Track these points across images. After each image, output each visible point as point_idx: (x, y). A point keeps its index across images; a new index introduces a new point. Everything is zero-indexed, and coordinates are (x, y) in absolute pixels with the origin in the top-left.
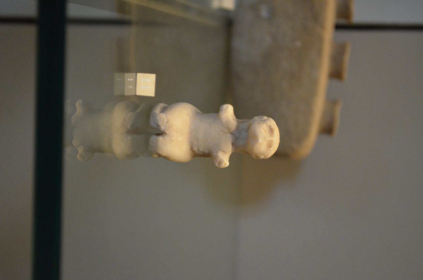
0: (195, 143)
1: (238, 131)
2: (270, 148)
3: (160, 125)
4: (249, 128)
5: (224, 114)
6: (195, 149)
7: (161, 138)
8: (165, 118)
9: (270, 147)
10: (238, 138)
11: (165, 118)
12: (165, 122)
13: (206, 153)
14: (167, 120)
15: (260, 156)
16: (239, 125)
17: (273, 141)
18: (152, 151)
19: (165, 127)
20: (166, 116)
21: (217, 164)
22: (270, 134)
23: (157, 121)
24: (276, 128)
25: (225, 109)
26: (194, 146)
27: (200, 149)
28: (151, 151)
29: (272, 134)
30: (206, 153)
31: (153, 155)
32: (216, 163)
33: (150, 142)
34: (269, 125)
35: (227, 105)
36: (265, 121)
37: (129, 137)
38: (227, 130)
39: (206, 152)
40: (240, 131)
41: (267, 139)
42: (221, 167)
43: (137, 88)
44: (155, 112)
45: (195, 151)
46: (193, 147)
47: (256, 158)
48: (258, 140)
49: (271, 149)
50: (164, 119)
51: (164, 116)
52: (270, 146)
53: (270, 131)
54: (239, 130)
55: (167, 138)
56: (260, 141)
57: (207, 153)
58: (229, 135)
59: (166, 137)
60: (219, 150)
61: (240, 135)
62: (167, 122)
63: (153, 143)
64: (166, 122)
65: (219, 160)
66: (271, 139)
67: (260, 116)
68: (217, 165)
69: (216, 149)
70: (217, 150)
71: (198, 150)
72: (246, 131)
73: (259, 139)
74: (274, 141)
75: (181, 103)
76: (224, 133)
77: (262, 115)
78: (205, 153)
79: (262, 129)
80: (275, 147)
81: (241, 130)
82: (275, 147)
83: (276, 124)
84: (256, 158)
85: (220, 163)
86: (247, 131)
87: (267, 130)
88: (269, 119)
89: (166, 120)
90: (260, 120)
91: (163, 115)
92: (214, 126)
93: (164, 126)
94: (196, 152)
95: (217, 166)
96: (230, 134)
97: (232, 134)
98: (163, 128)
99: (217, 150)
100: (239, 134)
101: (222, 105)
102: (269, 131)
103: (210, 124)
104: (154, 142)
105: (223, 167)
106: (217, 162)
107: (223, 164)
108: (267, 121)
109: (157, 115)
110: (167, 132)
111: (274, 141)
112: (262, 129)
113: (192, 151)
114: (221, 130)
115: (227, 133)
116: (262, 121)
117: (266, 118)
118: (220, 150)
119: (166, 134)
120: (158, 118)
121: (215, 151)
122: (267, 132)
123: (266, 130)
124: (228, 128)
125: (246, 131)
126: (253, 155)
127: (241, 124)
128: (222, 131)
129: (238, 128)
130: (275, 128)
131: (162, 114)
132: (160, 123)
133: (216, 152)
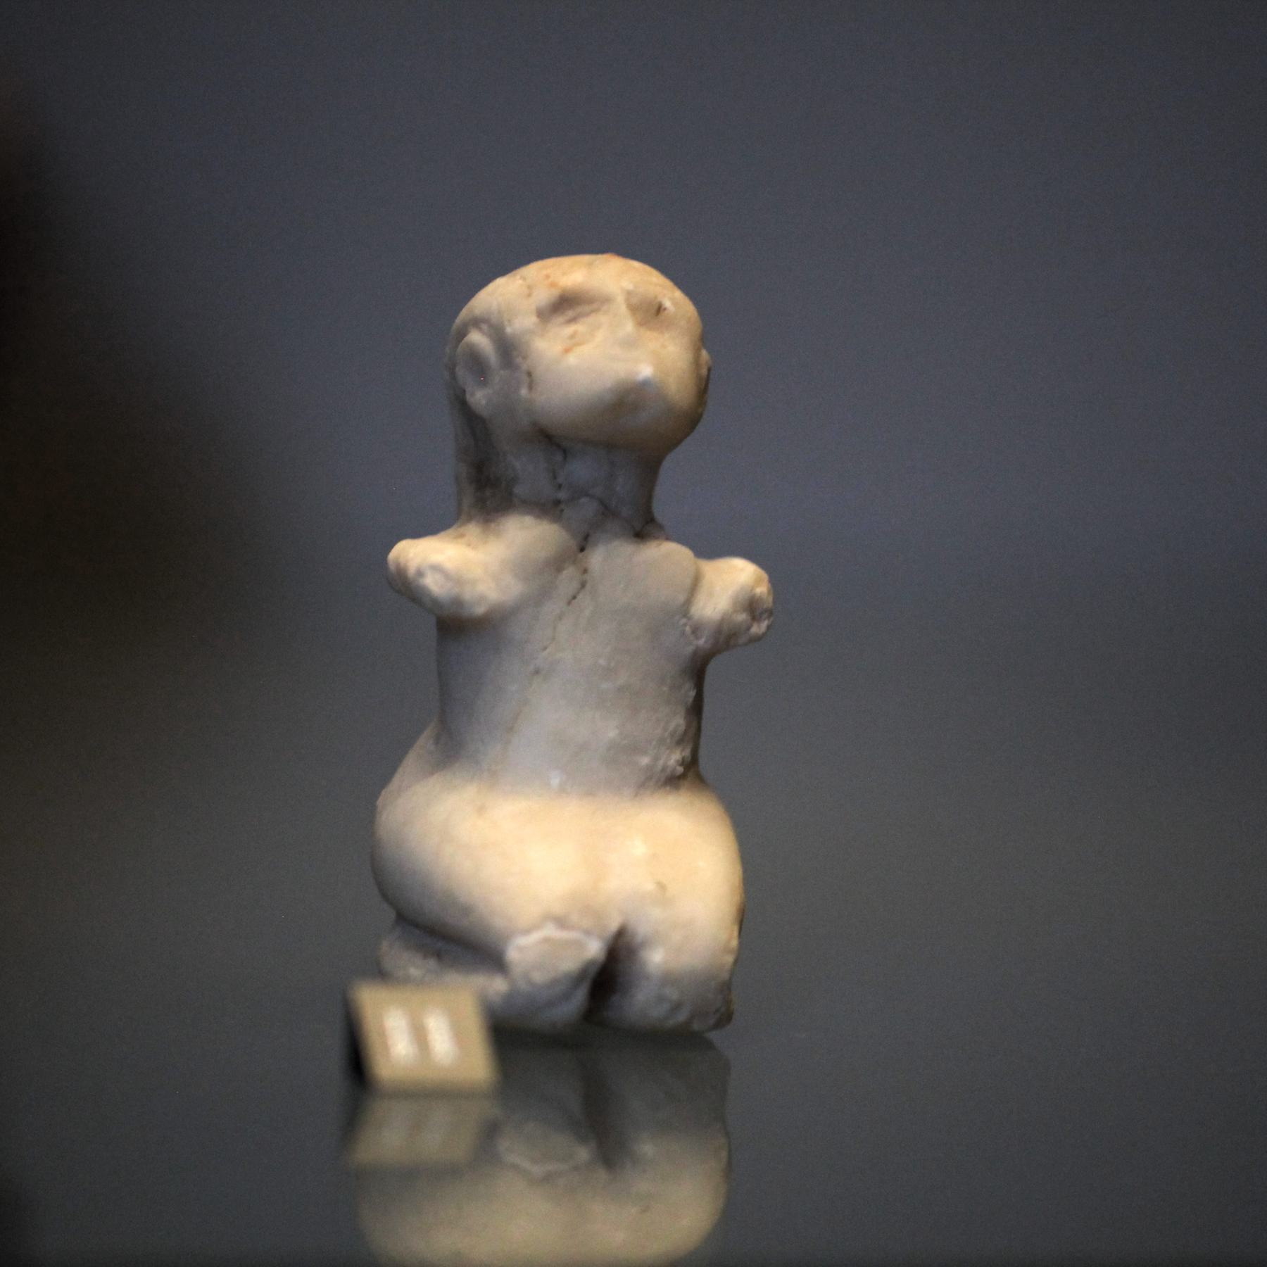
0: (645, 761)
1: (562, 506)
2: (665, 309)
6: (674, 758)
7: (656, 958)
8: (535, 937)
9: (660, 309)
11: (535, 937)
17: (629, 294)
18: (717, 1011)
19: (588, 933)
20: (527, 931)
24: (548, 277)
27: (675, 731)
33: (671, 1023)
37: (647, 1148)
40: (562, 495)
46: (663, 770)
48: (645, 384)
50: (546, 940)
51: (522, 941)
52: (650, 313)
53: (570, 313)
54: (557, 502)
55: (647, 921)
56: (645, 371)
58: (597, 558)
59: (642, 929)
61: (587, 495)
62: (561, 922)
63: (677, 1007)
65: (742, 617)
69: (683, 633)
70: (685, 625)
71: (680, 742)
72: (565, 458)
74: (630, 287)
75: (728, 822)
79: (572, 359)
81: (560, 486)
85: (752, 606)
87: (570, 329)
89: (550, 931)
91: (521, 949)
92: (545, 648)
95: (764, 624)
96: (586, 552)
97: (586, 538)
98: (594, 949)
100: (583, 500)
102: (573, 320)
103: (537, 672)
106: (749, 628)
110: (613, 926)
111: (627, 284)
112: (572, 359)
113: (683, 777)
114: (569, 603)
115: (585, 571)
118: (685, 609)
120: (539, 977)
122: (579, 327)
123: (572, 337)
124: (557, 564)
125: (565, 458)
127: (519, 490)
128: (574, 597)
129: (548, 508)
130: (553, 285)
132: (569, 963)
133: (696, 630)
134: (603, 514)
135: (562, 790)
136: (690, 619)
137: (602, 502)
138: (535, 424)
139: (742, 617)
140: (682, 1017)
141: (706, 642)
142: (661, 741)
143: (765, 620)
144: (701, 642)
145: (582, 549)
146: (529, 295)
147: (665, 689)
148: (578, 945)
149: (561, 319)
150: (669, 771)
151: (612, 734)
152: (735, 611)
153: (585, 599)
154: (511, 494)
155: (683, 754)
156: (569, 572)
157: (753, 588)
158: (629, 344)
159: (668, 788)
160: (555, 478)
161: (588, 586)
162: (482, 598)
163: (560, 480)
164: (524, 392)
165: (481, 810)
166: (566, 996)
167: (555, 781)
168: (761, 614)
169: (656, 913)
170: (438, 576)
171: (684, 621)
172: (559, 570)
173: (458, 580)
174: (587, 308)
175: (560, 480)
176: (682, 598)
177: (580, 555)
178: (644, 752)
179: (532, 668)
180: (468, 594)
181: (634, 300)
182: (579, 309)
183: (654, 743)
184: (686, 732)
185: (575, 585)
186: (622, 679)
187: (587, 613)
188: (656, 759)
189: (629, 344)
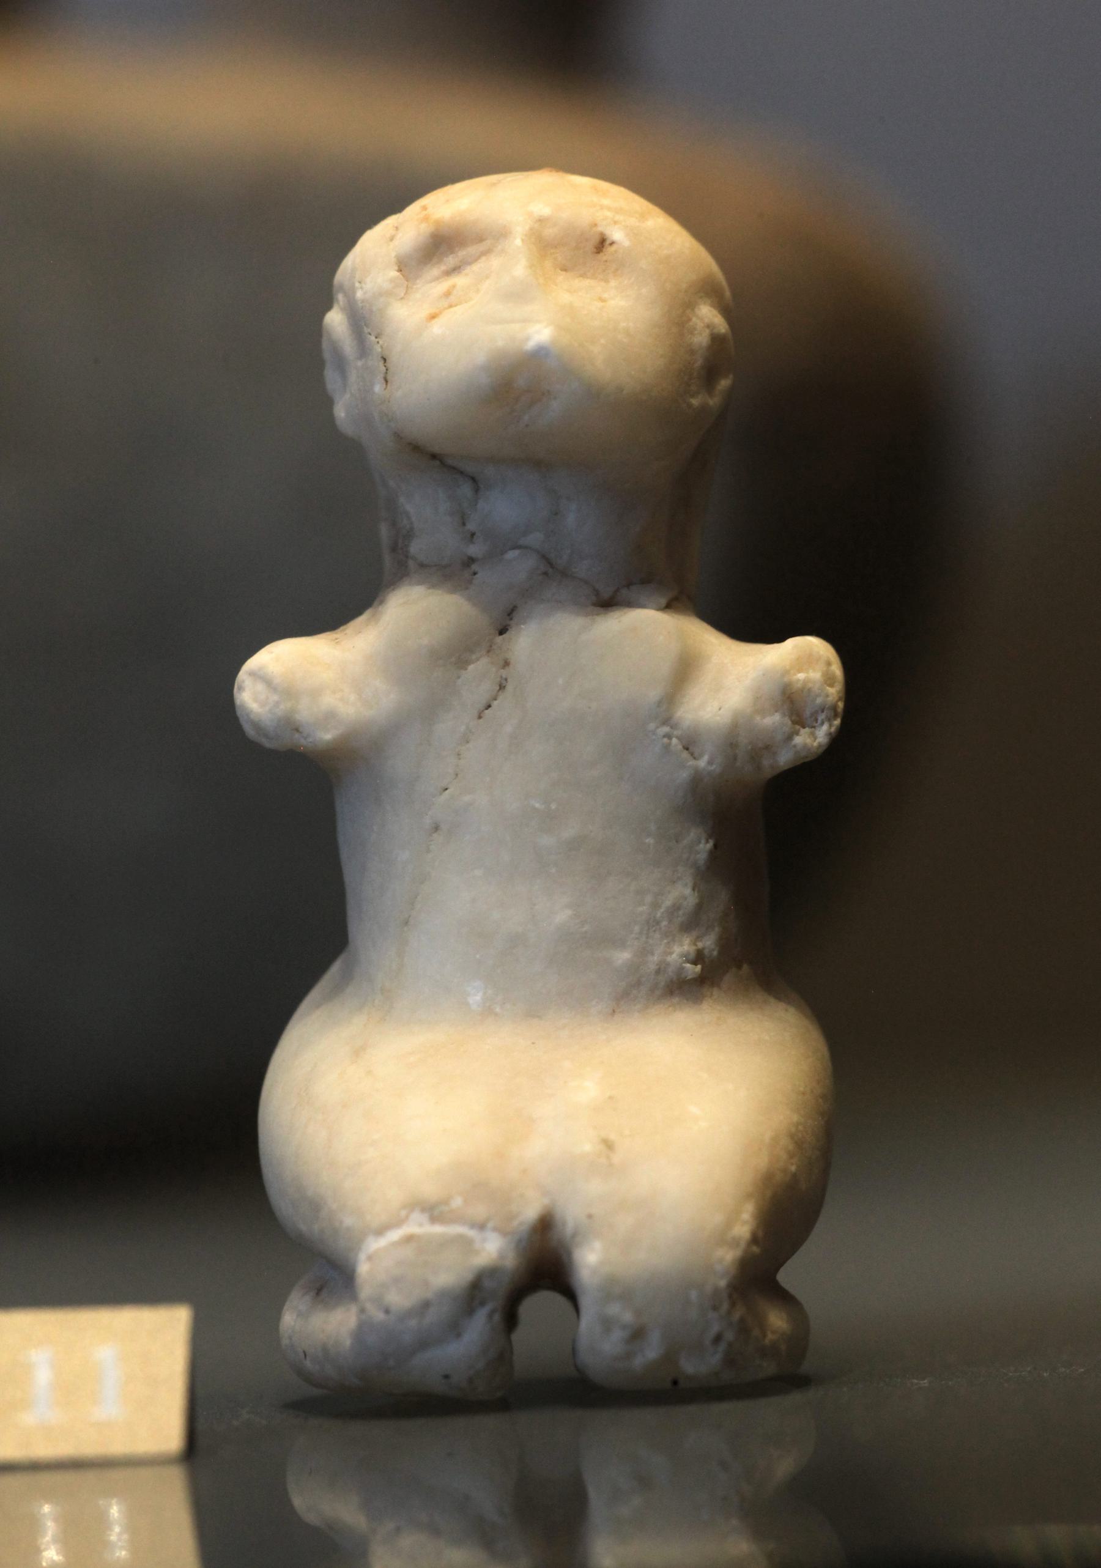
0: (623, 957)
1: (474, 567)
3: (469, 1277)
4: (434, 456)
5: (328, 701)
8: (394, 1235)
9: (602, 244)
10: (551, 564)
11: (394, 1235)
12: (438, 1229)
13: (715, 846)
14: (416, 1216)
15: (701, 339)
16: (422, 566)
17: (541, 220)
18: (718, 1339)
19: (481, 1227)
20: (380, 1232)
21: (805, 732)
22: (476, 259)
23: (426, 1305)
25: (275, 698)
26: (653, 967)
27: (675, 908)
28: (722, 1347)
29: (480, 239)
30: (710, 845)
31: (770, 1336)
32: (360, 290)
34: (393, 273)
35: (241, 688)
36: (359, 321)
38: (471, 667)
39: (705, 847)
41: (520, 269)
42: (834, 692)
43: (118, 1446)
44: (348, 1343)
45: (699, 958)
46: (658, 972)
47: (724, 383)
48: (540, 354)
49: (617, 235)
50: (409, 1239)
51: (375, 1244)
53: (451, 261)
54: (471, 560)
57: (710, 836)
59: (571, 1215)
60: (667, 721)
62: (434, 1211)
63: (637, 1335)
64: (434, 1220)
65: (773, 720)
66: (518, 242)
67: (330, 376)
68: (813, 734)
69: (667, 748)
70: (668, 736)
71: (692, 923)
72: (477, 490)
73: (531, 345)
76: (502, 687)
77: (321, 364)
78: (713, 855)
79: (437, 329)
80: (606, 202)
82: (606, 202)
83: (391, 221)
84: (724, 383)
86: (473, 479)
88: (341, 288)
89: (418, 1226)
90: (360, 363)
91: (370, 1258)
93: (471, 1233)
94: (709, 943)
97: (511, 612)
99: (674, 741)
100: (511, 555)
101: (239, 713)
102: (456, 270)
103: (436, 828)
104: (628, 1317)
105: (829, 680)
106: (789, 737)
107: (801, 676)
108: (359, 294)
109: (379, 1316)
110: (530, 1213)
111: (542, 209)
112: (437, 329)
115: (506, 664)
116: (363, 349)
117: (335, 319)
119: (545, 1225)
120: (398, 1300)
121: (685, 754)
122: (460, 281)
123: (448, 294)
125: (477, 490)
126: (695, 402)
127: (415, 548)
128: (489, 706)
131: (363, 1269)
134: (545, 574)
135: (488, 1011)
136: (673, 727)
137: (544, 557)
138: (398, 436)
139: (773, 720)
140: (651, 1351)
141: (710, 763)
142: (652, 923)
143: (822, 724)
144: (702, 763)
145: (502, 632)
146: (392, 239)
147: (650, 841)
148: (465, 1243)
149: (435, 271)
150: (671, 971)
151: (563, 916)
152: (762, 712)
153: (504, 704)
154: (407, 556)
155: (700, 945)
156: (480, 667)
157: (786, 672)
158: (516, 295)
159: (676, 1000)
160: (464, 524)
161: (510, 687)
162: (330, 716)
163: (471, 526)
164: (378, 388)
165: (358, 1053)
166: (454, 1328)
167: (476, 999)
168: (814, 716)
169: (595, 1187)
170: (260, 687)
171: (666, 729)
172: (462, 663)
173: (288, 692)
174: (472, 250)
175: (471, 526)
176: (654, 694)
177: (499, 639)
178: (621, 944)
179: (427, 821)
180: (305, 712)
181: (549, 232)
182: (462, 253)
183: (637, 928)
184: (699, 907)
185: (486, 688)
186: (569, 832)
187: (509, 729)
188: (644, 952)
189: (516, 295)
